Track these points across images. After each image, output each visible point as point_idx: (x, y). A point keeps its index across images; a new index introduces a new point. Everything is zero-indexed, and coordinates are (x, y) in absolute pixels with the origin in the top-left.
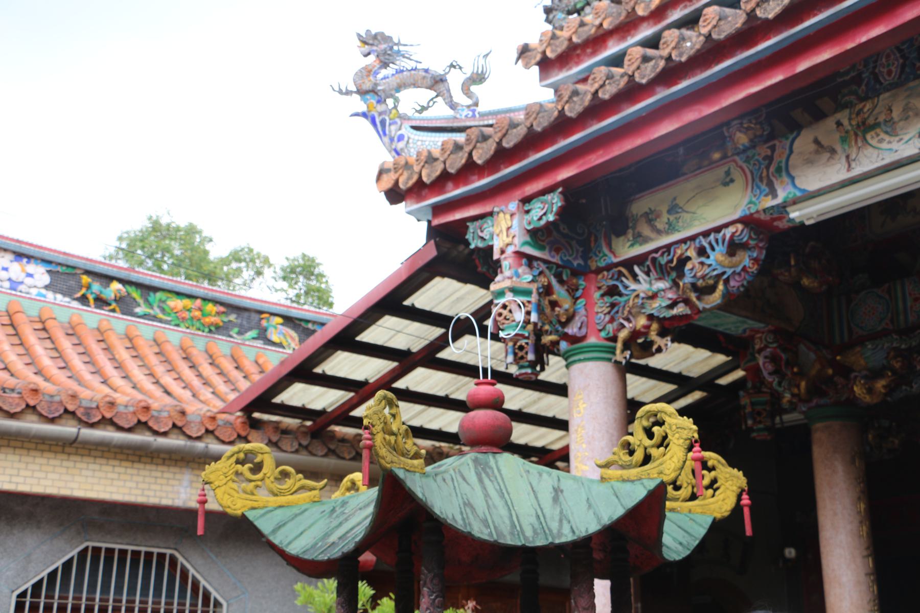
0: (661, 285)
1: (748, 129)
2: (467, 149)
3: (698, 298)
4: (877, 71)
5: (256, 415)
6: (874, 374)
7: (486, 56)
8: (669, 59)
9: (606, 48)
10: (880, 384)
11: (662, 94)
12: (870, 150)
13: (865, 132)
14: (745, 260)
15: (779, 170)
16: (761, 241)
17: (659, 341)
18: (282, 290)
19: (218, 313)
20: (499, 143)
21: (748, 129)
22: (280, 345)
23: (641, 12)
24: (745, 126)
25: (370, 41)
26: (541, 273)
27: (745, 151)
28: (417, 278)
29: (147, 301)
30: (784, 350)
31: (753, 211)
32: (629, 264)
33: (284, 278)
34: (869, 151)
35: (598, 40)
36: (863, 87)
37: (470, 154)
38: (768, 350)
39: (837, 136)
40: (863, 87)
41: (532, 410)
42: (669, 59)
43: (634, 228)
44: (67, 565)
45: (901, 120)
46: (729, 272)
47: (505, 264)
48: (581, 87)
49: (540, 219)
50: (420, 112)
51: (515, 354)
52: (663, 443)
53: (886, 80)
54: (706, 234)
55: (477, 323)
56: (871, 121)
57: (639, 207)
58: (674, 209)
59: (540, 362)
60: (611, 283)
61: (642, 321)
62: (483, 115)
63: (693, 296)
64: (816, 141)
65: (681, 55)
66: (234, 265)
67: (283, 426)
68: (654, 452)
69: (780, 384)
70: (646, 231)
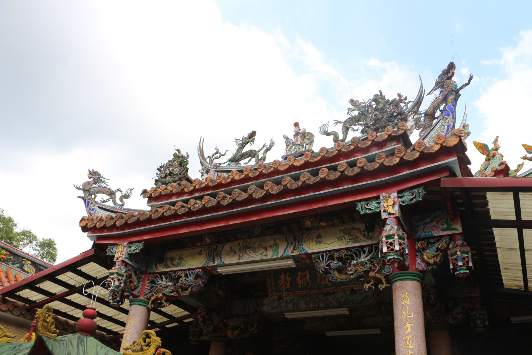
0: (170, 284)
1: (211, 238)
2: (115, 220)
3: (182, 291)
5: (7, 298)
7: (131, 190)
8: (190, 208)
9: (172, 199)
10: (236, 332)
11: (185, 219)
13: (246, 249)
14: (200, 282)
15: (217, 254)
17: (165, 304)
18: (38, 250)
19: (6, 255)
20: (126, 221)
21: (211, 238)
22: (27, 272)
23: (186, 190)
26: (129, 270)
27: (208, 245)
28: (85, 259)
32: (161, 274)
33: (40, 246)
35: (170, 195)
37: (115, 222)
41: (115, 317)
42: (190, 208)
43: (166, 262)
46: (194, 285)
47: (117, 263)
48: (159, 209)
49: (134, 251)
50: (103, 202)
51: (113, 297)
52: (149, 345)
54: (189, 270)
55: (101, 282)
56: (249, 246)
57: (169, 255)
58: (181, 259)
59: (122, 301)
60: (153, 279)
61: (160, 295)
62: (125, 209)
63: (180, 290)
64: (231, 248)
65: (194, 208)
66: (22, 237)
67: (16, 304)
68: (145, 348)
69: (204, 326)
70: (170, 264)
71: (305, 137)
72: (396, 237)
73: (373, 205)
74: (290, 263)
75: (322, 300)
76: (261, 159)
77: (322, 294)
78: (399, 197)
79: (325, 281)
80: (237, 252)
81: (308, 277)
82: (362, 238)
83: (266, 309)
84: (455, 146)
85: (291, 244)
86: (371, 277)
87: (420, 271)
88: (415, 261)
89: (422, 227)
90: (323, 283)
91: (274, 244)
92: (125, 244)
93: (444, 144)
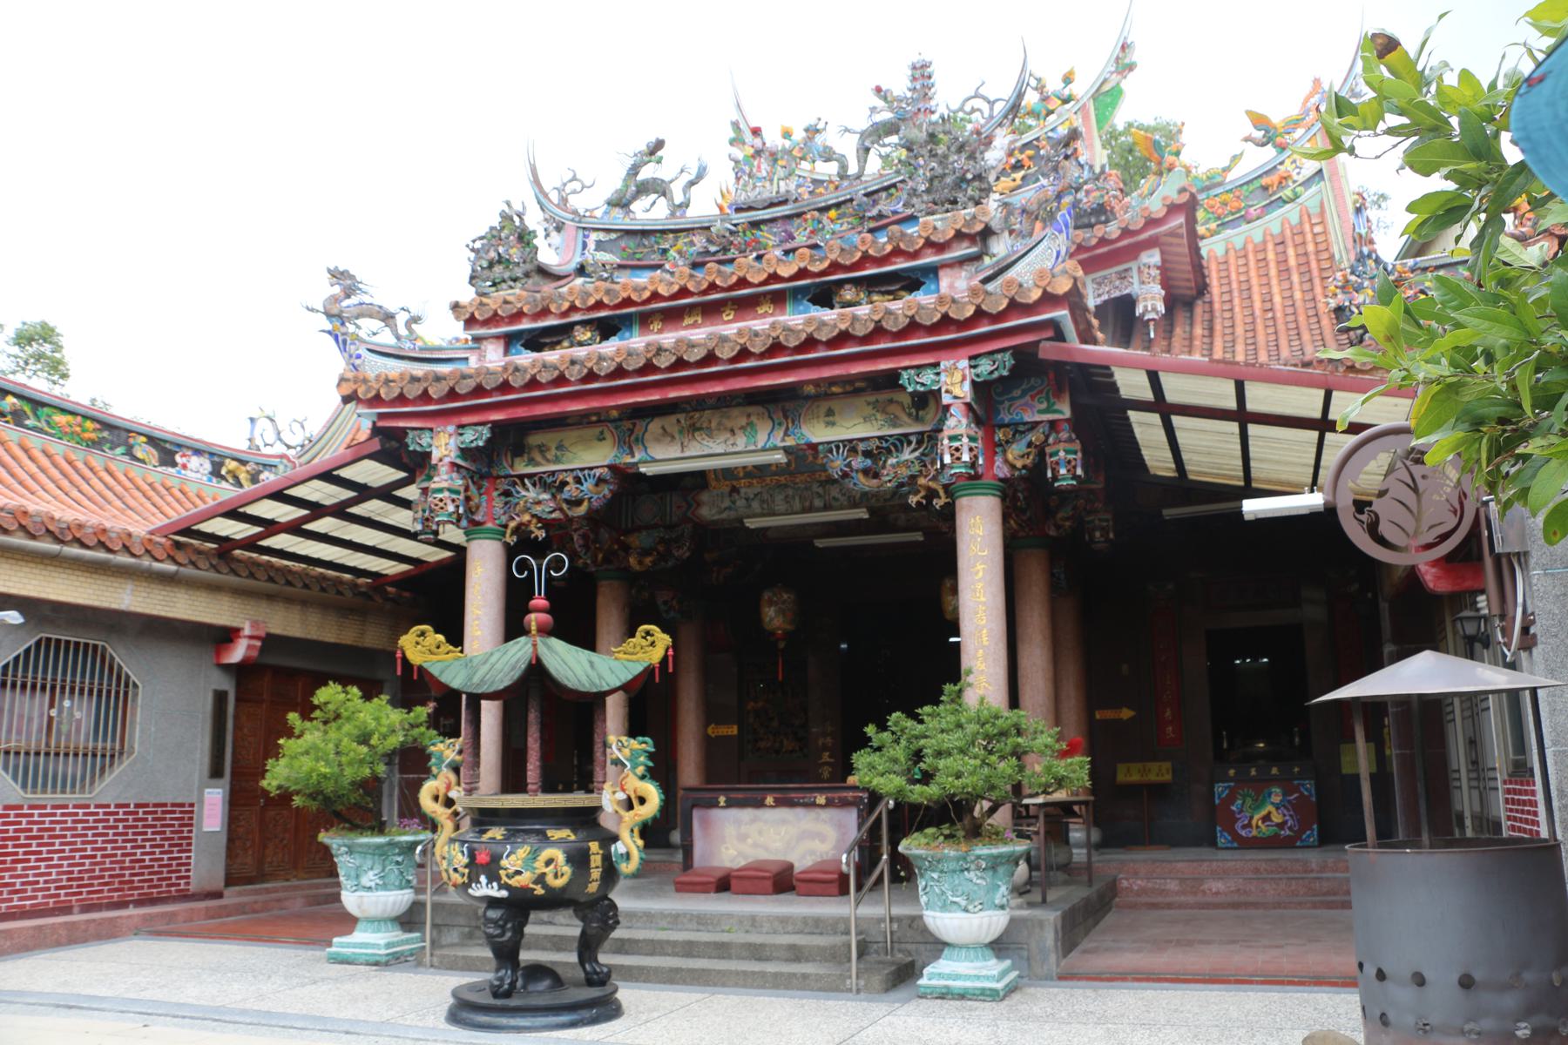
0: (546, 496)
6: (645, 552)
10: (648, 560)
15: (637, 440)
25: (337, 275)
29: (35, 415)
32: (522, 477)
44: (27, 651)
54: (582, 470)
58: (560, 447)
61: (526, 518)
70: (538, 458)
71: (775, 161)
72: (965, 440)
73: (928, 377)
74: (779, 457)
76: (680, 206)
78: (971, 367)
82: (905, 418)
83: (707, 513)
84: (1066, 295)
87: (1001, 480)
88: (993, 462)
89: (1007, 404)
92: (451, 428)
93: (1049, 289)
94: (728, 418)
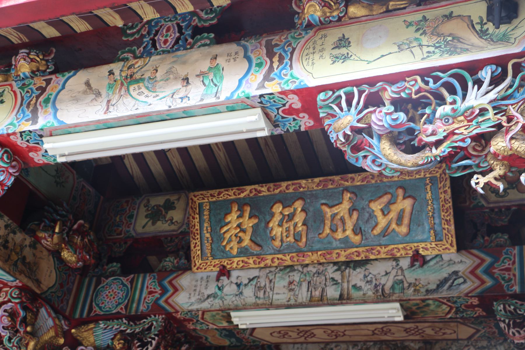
1: (32, 60)
4: (156, 38)
12: (130, 99)
13: (130, 84)
15: (47, 101)
16: (13, 167)
24: (32, 57)
30: (24, 308)
31: (10, 131)
34: (128, 100)
36: (141, 49)
38: (10, 304)
39: (106, 82)
40: (141, 49)
45: (161, 80)
53: (161, 47)
56: (137, 76)
64: (88, 84)
69: (10, 339)
75: (333, 279)
77: (335, 263)
79: (344, 231)
80: (104, 93)
81: (300, 218)
82: (475, 40)
85: (259, 65)
86: (495, 155)
90: (340, 235)
91: (210, 68)
94: (184, 63)
